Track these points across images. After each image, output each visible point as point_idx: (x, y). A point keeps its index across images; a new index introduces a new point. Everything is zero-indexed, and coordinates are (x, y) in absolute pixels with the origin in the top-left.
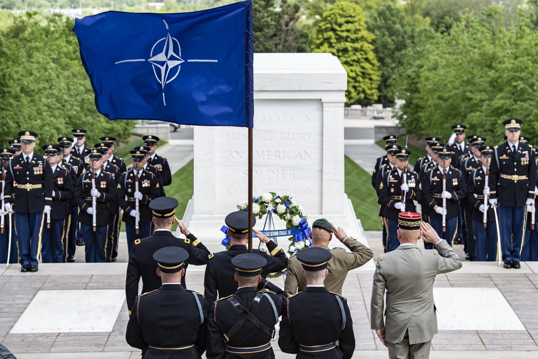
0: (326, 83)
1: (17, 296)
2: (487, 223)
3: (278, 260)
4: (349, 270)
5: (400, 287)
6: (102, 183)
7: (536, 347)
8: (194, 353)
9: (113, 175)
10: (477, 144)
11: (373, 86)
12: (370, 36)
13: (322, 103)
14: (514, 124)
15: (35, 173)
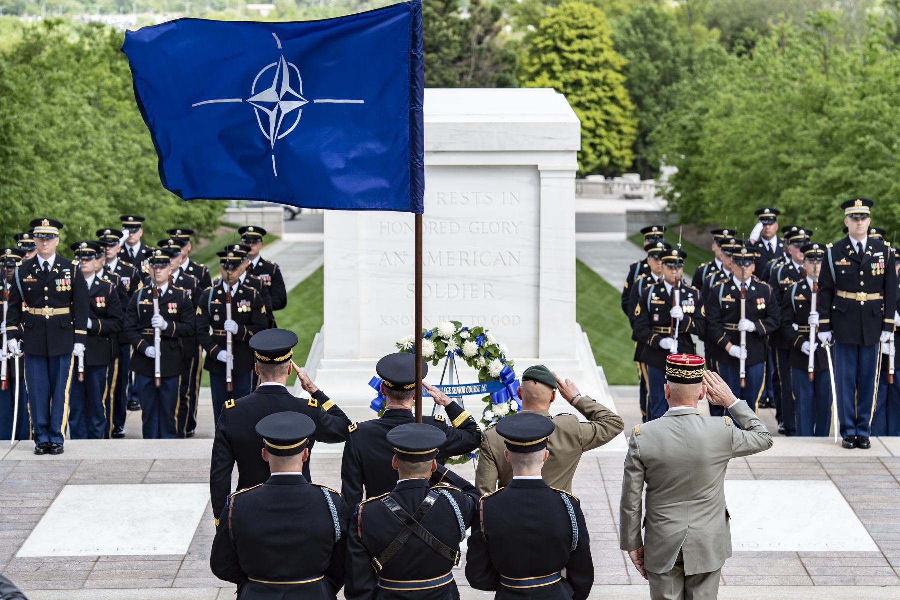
0: (545, 138)
1: (29, 495)
2: (815, 372)
3: (465, 434)
4: (584, 451)
5: (669, 479)
6: (170, 305)
7: (896, 580)
8: (324, 589)
9: (190, 292)
10: (798, 241)
11: (625, 143)
12: (620, 61)
13: (539, 172)
14: (859, 208)
15: (59, 289)
